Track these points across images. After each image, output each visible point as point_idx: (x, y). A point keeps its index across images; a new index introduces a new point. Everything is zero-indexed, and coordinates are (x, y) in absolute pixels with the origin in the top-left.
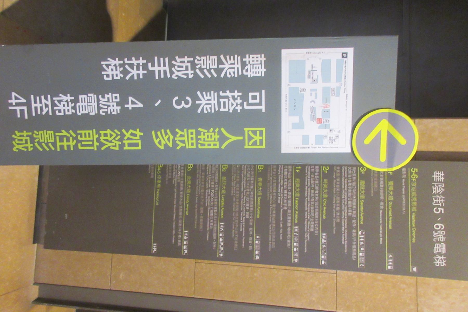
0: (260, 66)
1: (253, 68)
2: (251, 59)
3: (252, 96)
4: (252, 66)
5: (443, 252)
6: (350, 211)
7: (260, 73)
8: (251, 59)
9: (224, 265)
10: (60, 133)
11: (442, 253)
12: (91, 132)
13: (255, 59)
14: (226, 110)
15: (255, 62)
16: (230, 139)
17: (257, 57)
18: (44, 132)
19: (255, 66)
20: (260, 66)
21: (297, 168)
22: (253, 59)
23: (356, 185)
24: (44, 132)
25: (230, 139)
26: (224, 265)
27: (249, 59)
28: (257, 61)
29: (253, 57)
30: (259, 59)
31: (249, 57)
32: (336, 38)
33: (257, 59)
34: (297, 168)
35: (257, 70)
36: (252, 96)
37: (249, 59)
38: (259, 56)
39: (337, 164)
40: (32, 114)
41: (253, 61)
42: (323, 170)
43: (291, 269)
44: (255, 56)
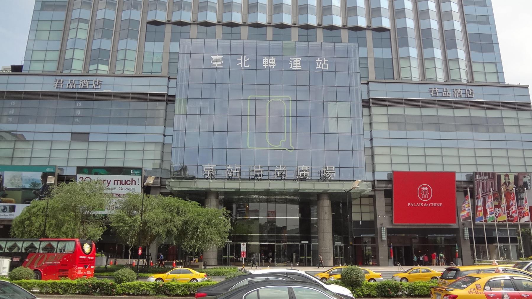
0: (270, 60)
1: (271, 63)
4: (269, 64)
6: (487, 153)
7: (274, 60)
9: (384, 71)
10: (447, 268)
12: (300, 65)
15: (268, 62)
17: (265, 61)
18: (300, 66)
19: (270, 62)
20: (270, 60)
22: (266, 63)
24: (300, 66)
26: (384, 71)
27: (266, 59)
29: (265, 63)
32: (240, 293)
35: (272, 61)
37: (266, 59)
42: (320, 62)
44: (264, 61)
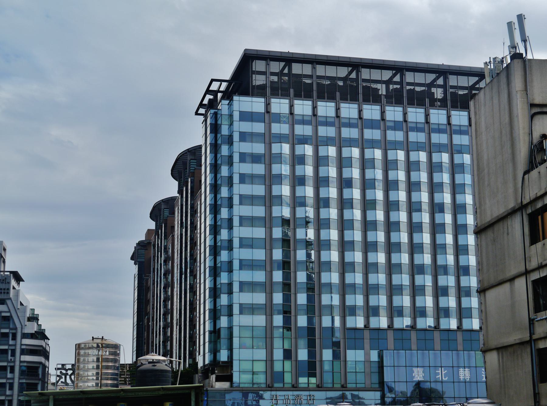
2: (462, 376)
3: (444, 378)
5: (422, 375)
8: (462, 376)
11: (423, 375)
13: (461, 374)
14: (422, 372)
15: (463, 373)
16: (444, 372)
17: (462, 375)
21: (398, 86)
22: (462, 375)
23: (423, 373)
25: (444, 372)
28: (462, 372)
29: (461, 375)
30: (461, 371)
31: (461, 377)
33: (462, 375)
34: (398, 86)
36: (444, 378)
38: (460, 371)
39: (150, 358)
40: (446, 372)
41: (462, 375)
43: (332, 291)
